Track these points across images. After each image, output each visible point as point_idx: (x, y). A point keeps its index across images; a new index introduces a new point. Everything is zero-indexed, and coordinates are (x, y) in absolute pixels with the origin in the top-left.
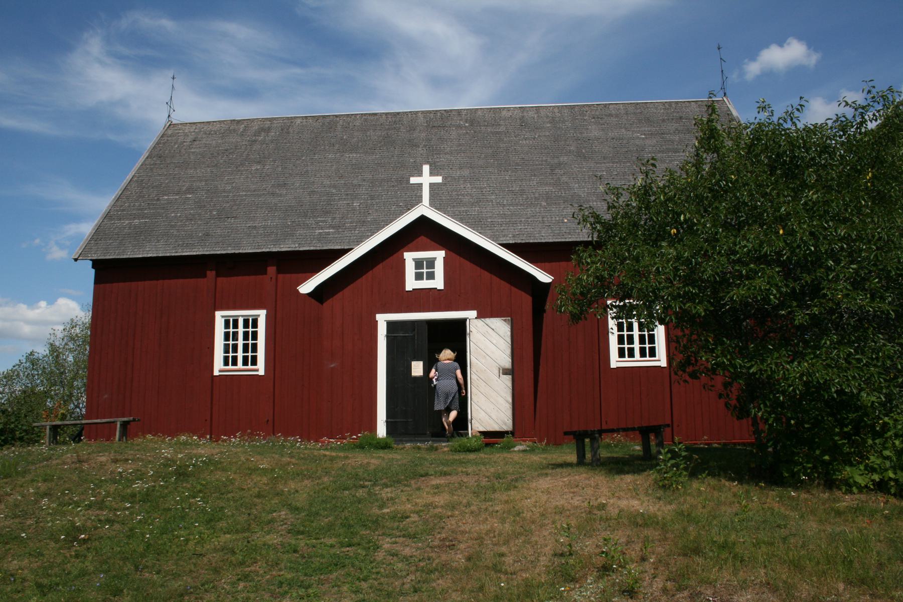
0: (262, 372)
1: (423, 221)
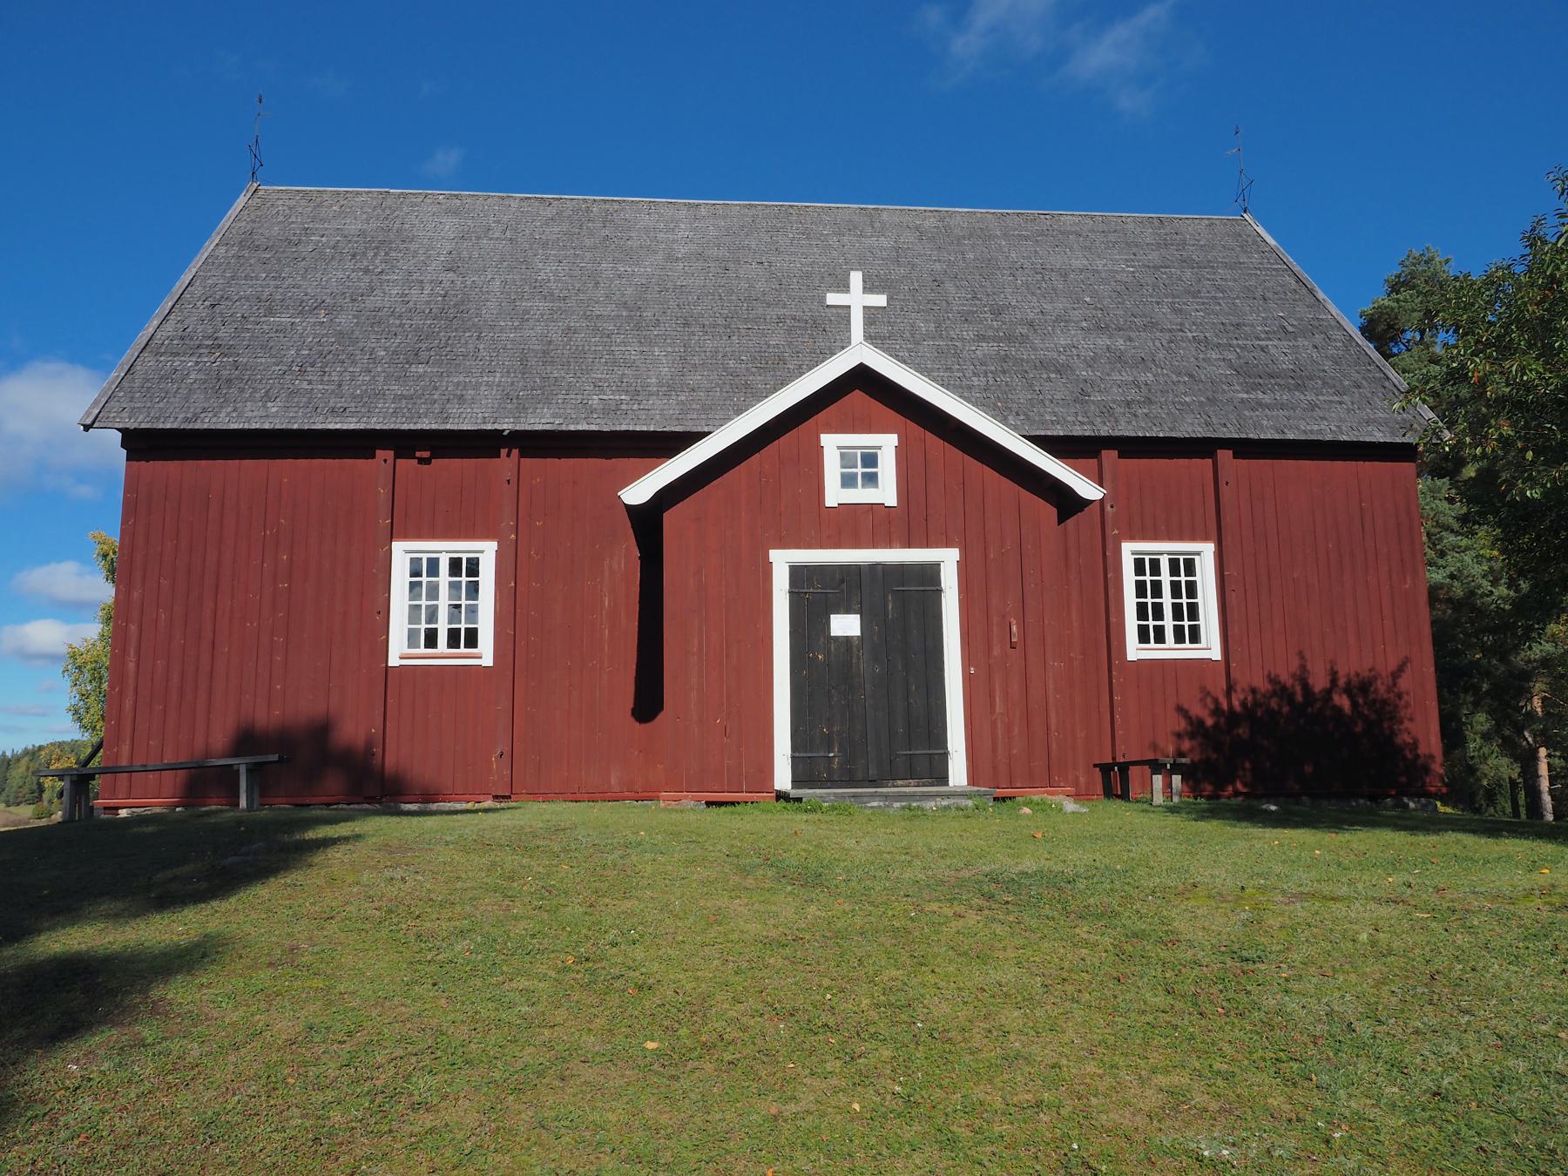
0: (487, 660)
1: (862, 378)
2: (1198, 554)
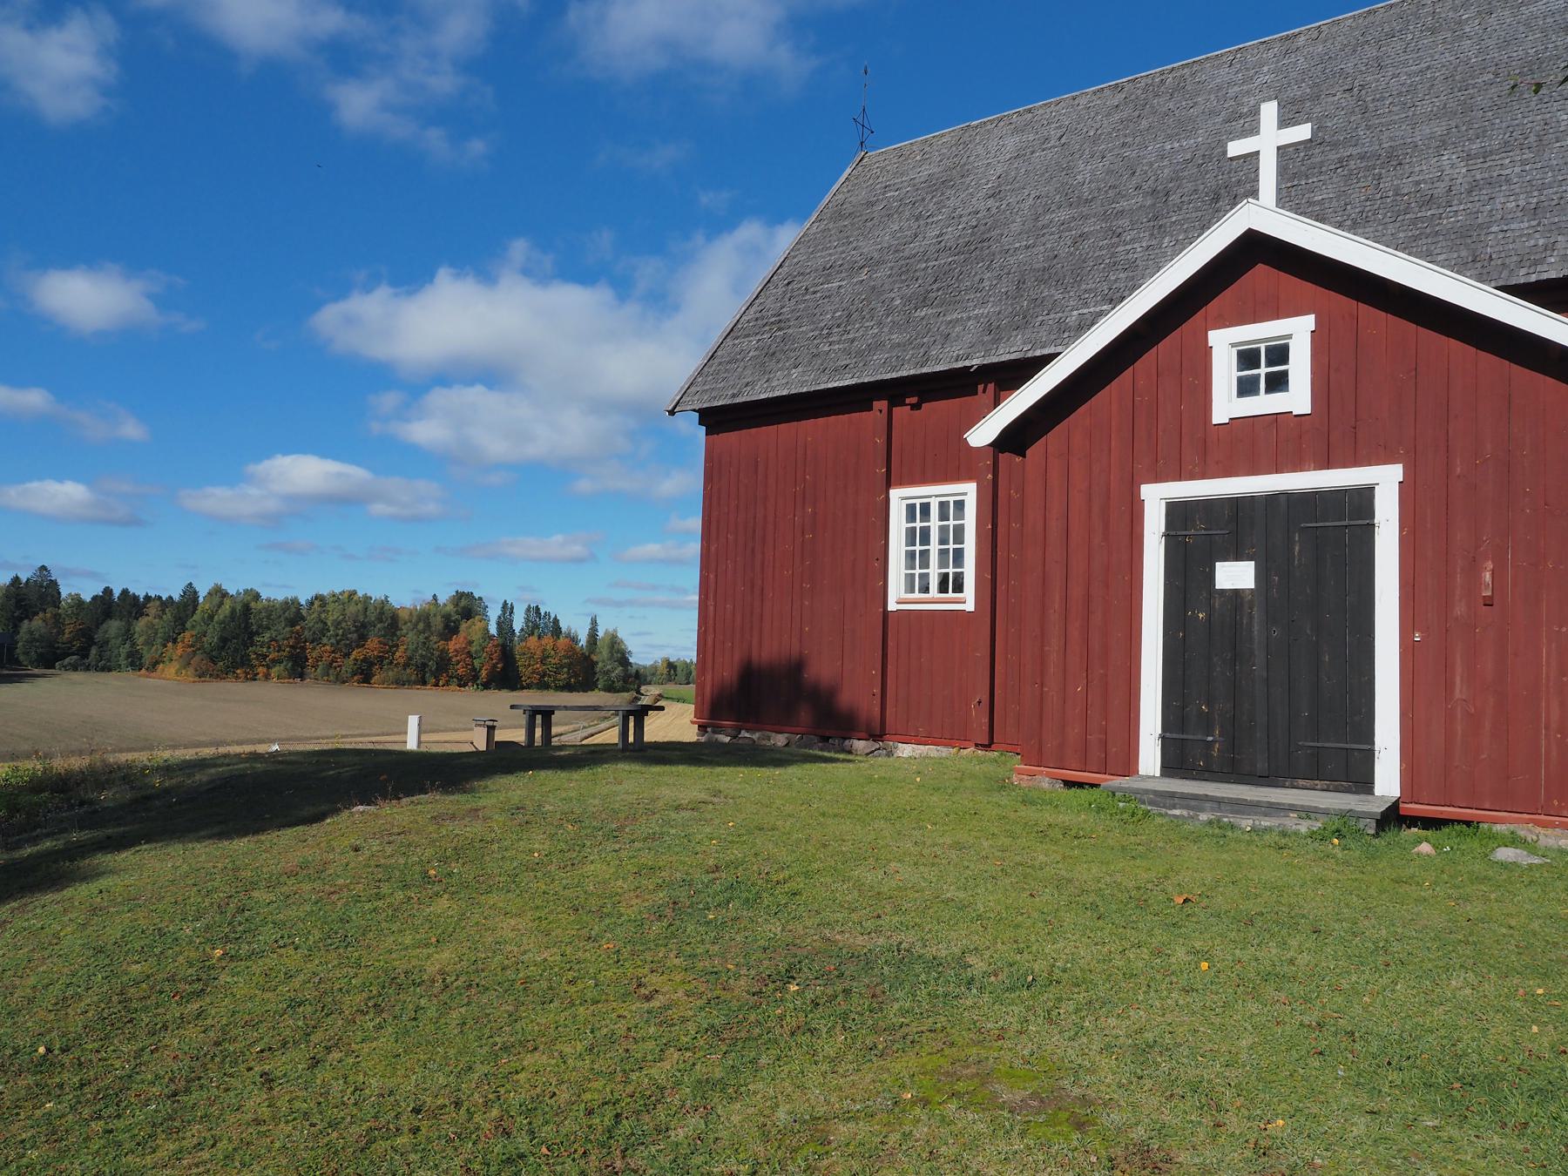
0: (970, 606)
1: (1255, 249)
2: (1290, 336)
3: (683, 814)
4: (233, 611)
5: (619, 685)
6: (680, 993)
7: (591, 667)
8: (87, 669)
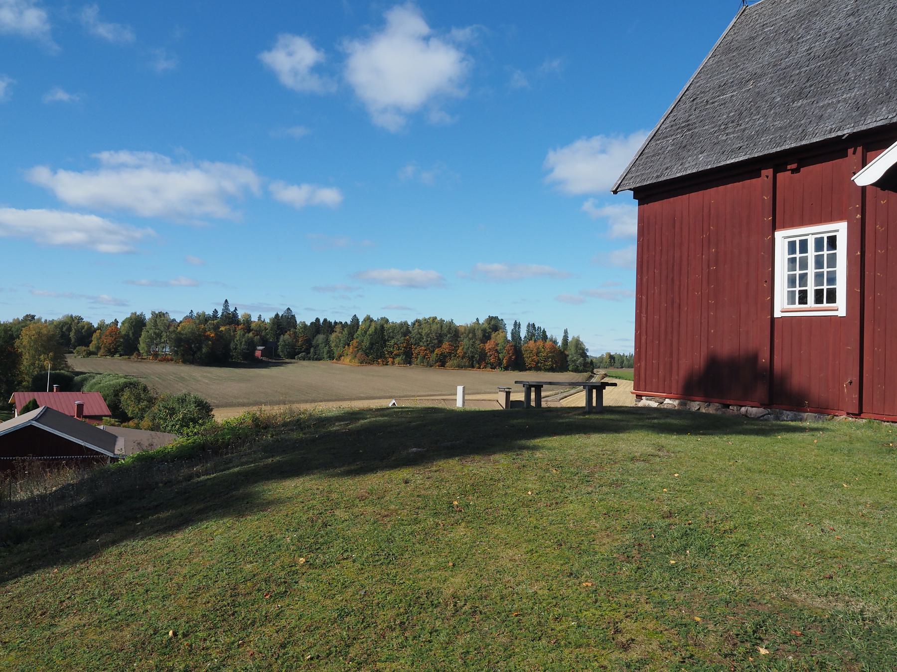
0: (842, 312)
2: (837, 231)
3: (637, 464)
4: (376, 329)
5: (581, 368)
6: (655, 645)
7: (566, 358)
8: (309, 359)
